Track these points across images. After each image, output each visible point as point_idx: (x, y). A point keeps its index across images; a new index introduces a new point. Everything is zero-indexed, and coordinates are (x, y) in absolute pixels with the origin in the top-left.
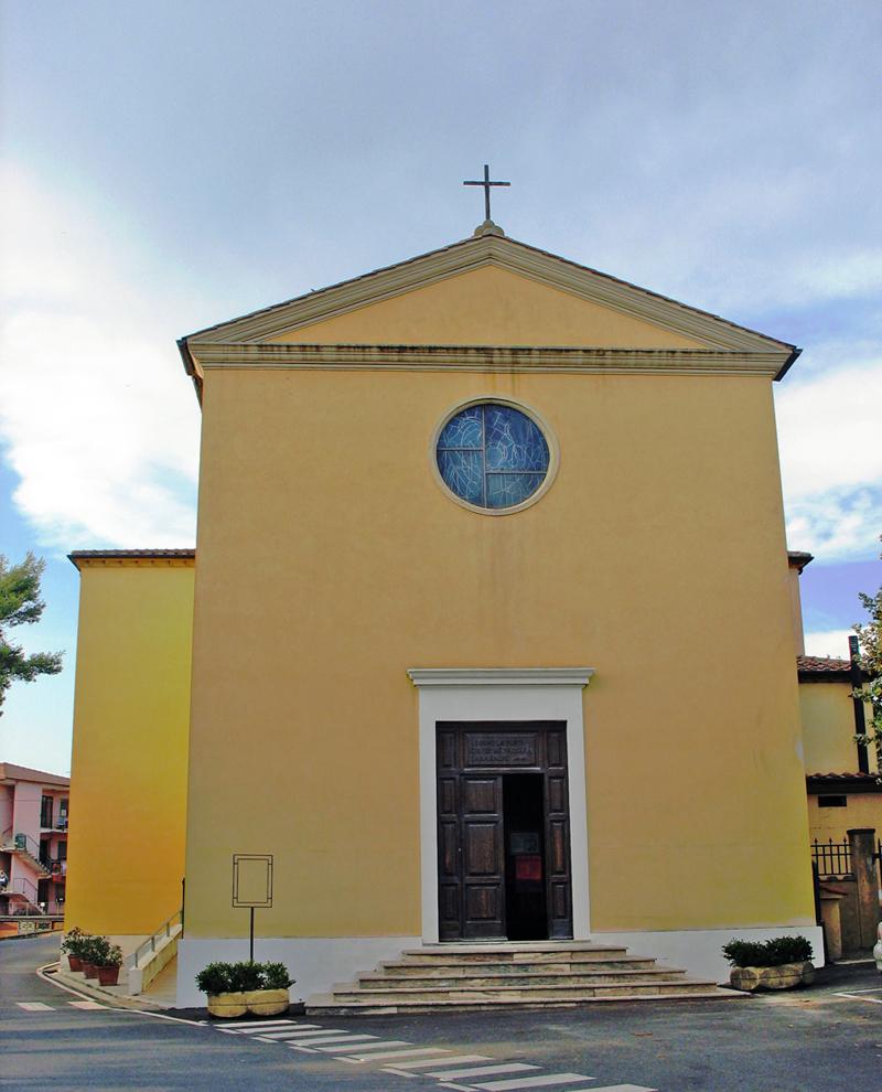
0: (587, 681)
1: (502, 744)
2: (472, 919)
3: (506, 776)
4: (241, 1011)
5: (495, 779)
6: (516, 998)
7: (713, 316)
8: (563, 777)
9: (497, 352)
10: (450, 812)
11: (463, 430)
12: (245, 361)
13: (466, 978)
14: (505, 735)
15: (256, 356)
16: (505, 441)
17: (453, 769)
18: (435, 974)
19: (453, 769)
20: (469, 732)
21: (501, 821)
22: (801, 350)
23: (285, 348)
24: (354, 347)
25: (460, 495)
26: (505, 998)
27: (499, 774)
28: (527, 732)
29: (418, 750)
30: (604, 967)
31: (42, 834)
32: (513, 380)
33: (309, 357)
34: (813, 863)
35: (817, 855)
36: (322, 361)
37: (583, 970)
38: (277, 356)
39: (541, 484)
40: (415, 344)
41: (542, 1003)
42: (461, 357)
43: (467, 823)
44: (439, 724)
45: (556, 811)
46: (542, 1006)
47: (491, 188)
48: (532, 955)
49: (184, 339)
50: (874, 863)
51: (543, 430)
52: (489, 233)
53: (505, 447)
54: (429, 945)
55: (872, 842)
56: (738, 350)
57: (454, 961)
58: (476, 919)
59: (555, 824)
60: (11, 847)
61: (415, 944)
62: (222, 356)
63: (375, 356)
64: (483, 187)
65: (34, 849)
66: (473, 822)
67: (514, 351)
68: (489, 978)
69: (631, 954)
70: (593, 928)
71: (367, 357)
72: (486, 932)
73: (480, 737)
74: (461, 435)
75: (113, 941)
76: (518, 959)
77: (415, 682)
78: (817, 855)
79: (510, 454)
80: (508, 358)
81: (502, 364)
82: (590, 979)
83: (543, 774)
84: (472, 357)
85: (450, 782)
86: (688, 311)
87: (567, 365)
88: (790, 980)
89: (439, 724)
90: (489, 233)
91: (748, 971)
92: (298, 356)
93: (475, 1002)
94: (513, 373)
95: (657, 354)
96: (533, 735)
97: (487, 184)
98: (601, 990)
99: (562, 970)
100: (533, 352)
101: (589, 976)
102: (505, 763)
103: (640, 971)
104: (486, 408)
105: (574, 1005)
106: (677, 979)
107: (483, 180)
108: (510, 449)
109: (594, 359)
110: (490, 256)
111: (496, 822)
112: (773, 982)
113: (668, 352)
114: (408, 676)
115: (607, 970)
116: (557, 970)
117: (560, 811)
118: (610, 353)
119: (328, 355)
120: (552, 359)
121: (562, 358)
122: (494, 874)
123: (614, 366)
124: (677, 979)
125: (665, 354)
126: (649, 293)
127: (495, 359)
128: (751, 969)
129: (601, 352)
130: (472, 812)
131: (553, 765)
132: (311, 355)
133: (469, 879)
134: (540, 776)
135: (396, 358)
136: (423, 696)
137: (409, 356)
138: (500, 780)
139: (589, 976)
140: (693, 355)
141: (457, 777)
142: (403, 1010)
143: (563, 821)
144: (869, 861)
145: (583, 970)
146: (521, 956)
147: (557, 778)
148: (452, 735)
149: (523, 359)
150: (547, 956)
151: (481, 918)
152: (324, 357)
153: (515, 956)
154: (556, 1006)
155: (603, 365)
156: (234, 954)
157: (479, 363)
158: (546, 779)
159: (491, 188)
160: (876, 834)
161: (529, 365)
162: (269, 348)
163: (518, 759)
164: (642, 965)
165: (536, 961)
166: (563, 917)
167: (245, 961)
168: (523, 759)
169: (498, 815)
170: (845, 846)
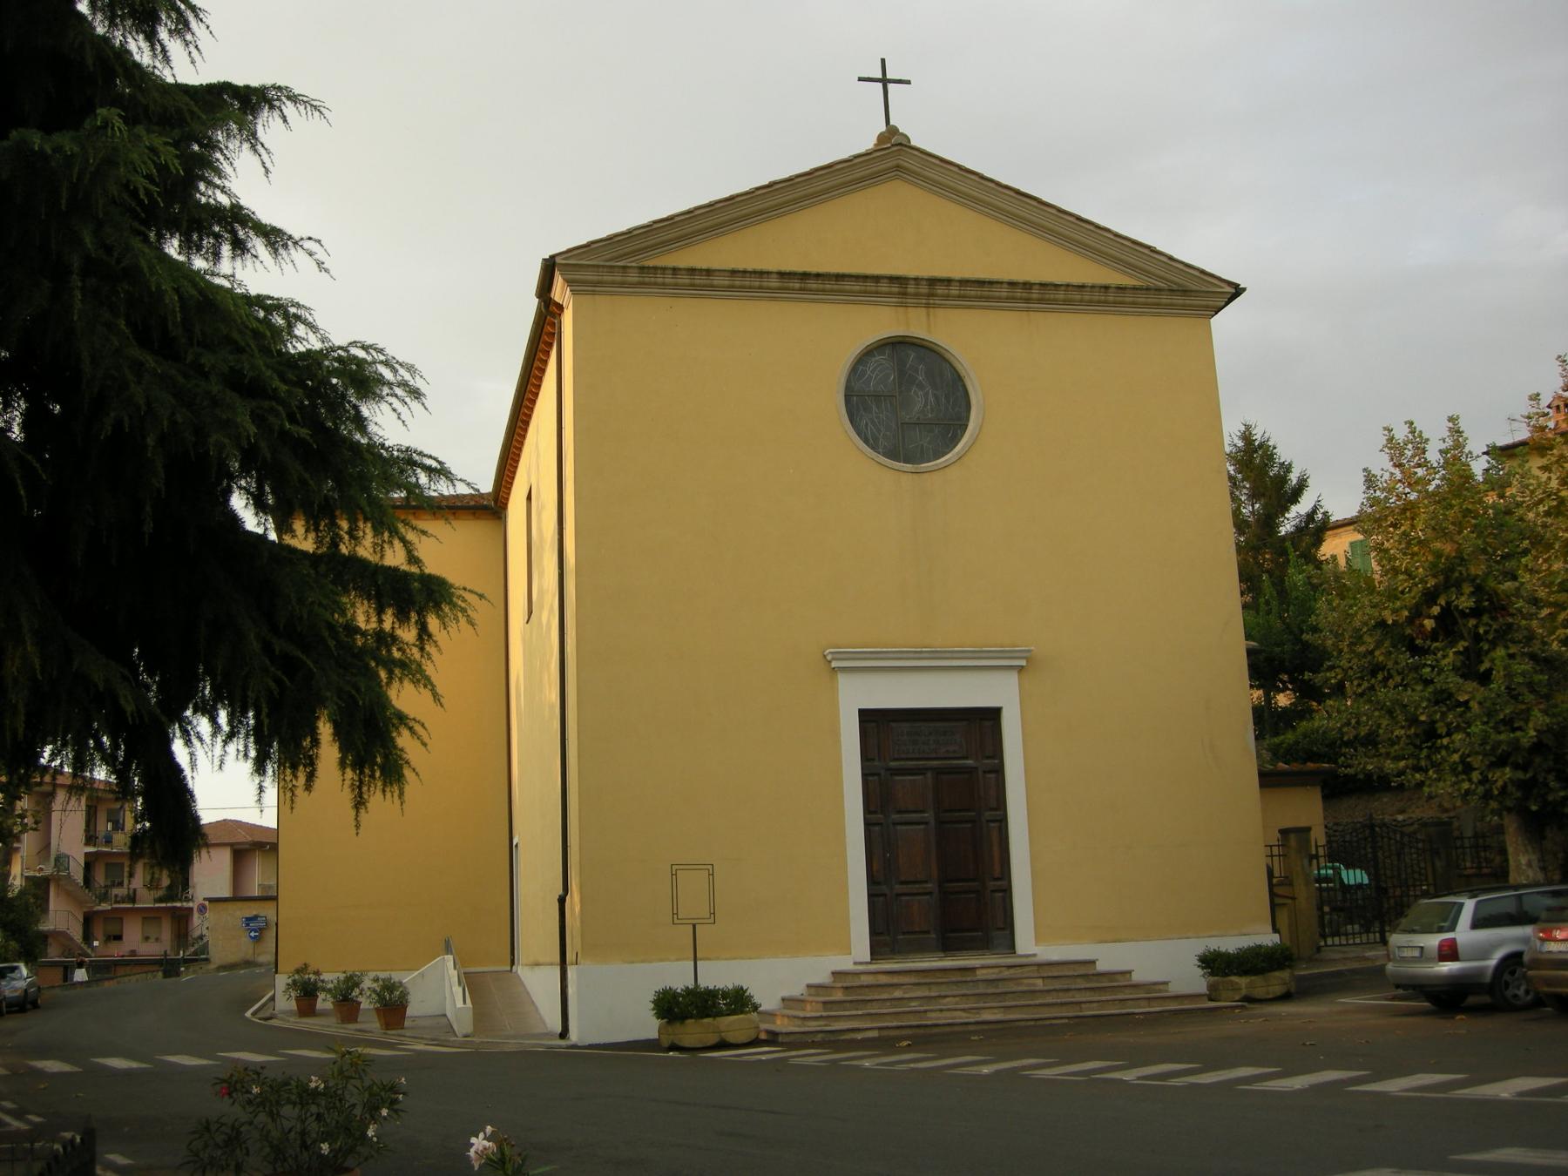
0: (1023, 663)
1: (930, 734)
2: (904, 933)
3: (938, 771)
4: (712, 1039)
5: (924, 774)
6: (999, 1016)
7: (1148, 247)
8: (999, 771)
9: (913, 282)
10: (875, 812)
11: (873, 372)
12: (622, 284)
13: (939, 997)
14: (932, 724)
15: (636, 279)
16: (921, 386)
17: (876, 763)
18: (898, 994)
19: (876, 763)
20: (893, 721)
21: (932, 822)
22: (1244, 289)
23: (670, 272)
24: (750, 272)
25: (873, 448)
26: (987, 1016)
27: (927, 769)
28: (957, 720)
29: (839, 741)
30: (1079, 980)
31: (87, 854)
32: (928, 315)
33: (697, 282)
34: (1268, 867)
35: (1272, 856)
36: (712, 287)
37: (1057, 985)
38: (660, 280)
39: (962, 436)
40: (821, 270)
41: (1032, 1020)
42: (871, 286)
43: (894, 824)
44: (862, 713)
45: (991, 809)
46: (1032, 1023)
47: (891, 86)
48: (996, 970)
49: (553, 257)
50: (1310, 864)
51: (963, 373)
52: (893, 143)
53: (920, 393)
54: (861, 963)
55: (1308, 841)
56: (1175, 287)
57: (913, 979)
58: (908, 933)
59: (992, 825)
60: (48, 870)
61: (845, 963)
62: (595, 278)
63: (774, 282)
64: (880, 85)
65: (78, 874)
66: (901, 824)
67: (933, 282)
68: (963, 995)
69: (1101, 967)
70: (1039, 939)
71: (765, 284)
72: (920, 948)
73: (905, 727)
74: (870, 377)
75: (396, 976)
76: (981, 974)
77: (834, 664)
78: (1272, 856)
79: (927, 399)
80: (924, 289)
81: (917, 295)
82: (1071, 994)
83: (976, 768)
84: (884, 287)
85: (876, 778)
86: (1084, 225)
87: (988, 299)
88: (1278, 990)
89: (862, 713)
90: (893, 143)
91: (1232, 982)
92: (685, 280)
93: (962, 1021)
94: (928, 306)
95: (1088, 289)
96: (965, 723)
97: (885, 81)
98: (1088, 1005)
99: (1034, 985)
100: (953, 284)
101: (1068, 990)
102: (934, 755)
103: (1115, 984)
104: (897, 345)
105: (1067, 1021)
106: (1160, 991)
107: (881, 77)
108: (926, 395)
109: (1019, 293)
110: (898, 168)
111: (926, 823)
112: (1259, 992)
113: (1101, 287)
114: (825, 656)
115: (1082, 984)
116: (1029, 985)
117: (996, 809)
118: (1037, 287)
119: (717, 281)
120: (971, 291)
121: (985, 291)
122: (926, 882)
123: (1040, 301)
124: (1160, 991)
125: (1097, 289)
126: (1018, 192)
127: (909, 290)
128: (1234, 979)
129: (1027, 286)
130: (899, 812)
131: (988, 758)
132: (701, 282)
133: (898, 888)
134: (971, 771)
135: (797, 286)
136: (842, 679)
137: (812, 284)
138: (929, 775)
139: (1068, 990)
140: (1128, 291)
141: (883, 772)
142: (885, 1033)
143: (1000, 821)
144: (1306, 862)
145: (1057, 985)
146: (984, 971)
147: (990, 772)
148: (874, 724)
149: (940, 290)
150: (1012, 971)
151: (915, 933)
152: (715, 282)
153: (978, 972)
154: (1048, 1022)
155: (1028, 300)
156: (678, 977)
157: (890, 294)
158: (980, 773)
159: (891, 86)
160: (1312, 833)
161: (947, 297)
162: (652, 271)
163: (947, 751)
164: (1118, 977)
165: (1000, 976)
166: (1003, 929)
167: (691, 985)
168: (954, 752)
169: (929, 815)
170: (1279, 846)
